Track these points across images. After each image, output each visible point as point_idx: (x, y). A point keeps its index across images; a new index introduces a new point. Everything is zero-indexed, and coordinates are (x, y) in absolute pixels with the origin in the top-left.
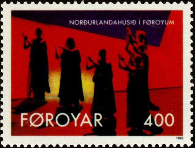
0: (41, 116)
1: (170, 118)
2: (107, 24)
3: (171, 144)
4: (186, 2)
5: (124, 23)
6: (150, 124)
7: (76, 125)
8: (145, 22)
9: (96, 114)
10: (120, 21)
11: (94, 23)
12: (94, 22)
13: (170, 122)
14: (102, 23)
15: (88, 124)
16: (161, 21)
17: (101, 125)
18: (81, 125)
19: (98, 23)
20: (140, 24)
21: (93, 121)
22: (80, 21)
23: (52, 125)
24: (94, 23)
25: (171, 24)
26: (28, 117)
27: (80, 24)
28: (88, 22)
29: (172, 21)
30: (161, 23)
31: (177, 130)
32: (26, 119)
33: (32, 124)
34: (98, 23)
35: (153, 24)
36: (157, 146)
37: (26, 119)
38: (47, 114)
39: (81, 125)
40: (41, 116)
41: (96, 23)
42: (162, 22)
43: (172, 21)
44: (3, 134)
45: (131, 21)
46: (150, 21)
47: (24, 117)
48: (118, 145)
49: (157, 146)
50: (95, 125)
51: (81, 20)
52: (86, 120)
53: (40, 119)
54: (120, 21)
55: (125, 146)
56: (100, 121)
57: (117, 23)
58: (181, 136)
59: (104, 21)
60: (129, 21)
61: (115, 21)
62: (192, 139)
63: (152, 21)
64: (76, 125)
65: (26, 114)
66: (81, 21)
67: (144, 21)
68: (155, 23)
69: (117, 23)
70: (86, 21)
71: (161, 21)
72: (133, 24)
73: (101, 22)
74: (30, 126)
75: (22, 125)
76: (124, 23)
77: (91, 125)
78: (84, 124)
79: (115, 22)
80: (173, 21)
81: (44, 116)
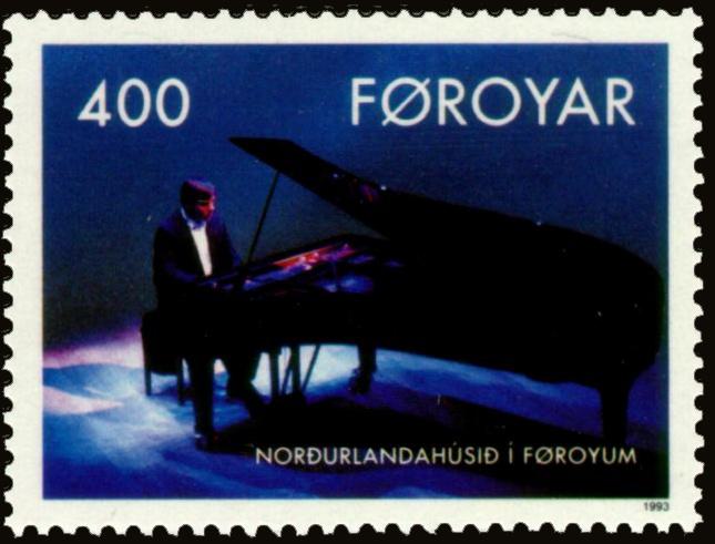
0: (421, 87)
1: (173, 95)
2: (393, 460)
5: (455, 458)
6: (102, 117)
7: (542, 120)
8: (530, 455)
9: (612, 83)
10: (439, 451)
11: (344, 457)
12: (344, 455)
13: (172, 110)
14: (374, 459)
15: (585, 117)
16: (590, 450)
17: (629, 120)
18: (561, 120)
19: (361, 458)
20: (511, 461)
21: (600, 109)
22: (293, 451)
23: (462, 121)
24: (344, 457)
25: (623, 459)
26: (375, 91)
27: (293, 459)
28: (323, 455)
29: (627, 452)
30: (589, 456)
32: (370, 99)
33: (391, 117)
34: (361, 458)
35: (299, 462)
37: (370, 99)
38: (443, 83)
39: (561, 120)
40: (421, 87)
41: (351, 458)
42: (594, 455)
43: (627, 452)
45: (480, 451)
46: (550, 451)
47: (364, 90)
50: (610, 120)
51: (298, 446)
52: (578, 102)
53: (419, 98)
54: (439, 451)
56: (628, 107)
57: (430, 457)
58: (662, 501)
59: (383, 452)
60: (470, 451)
61: (422, 451)
63: (558, 449)
64: (542, 120)
65: (370, 81)
66: (561, 452)
67: (526, 449)
68: (566, 457)
69: (430, 457)
70: (314, 449)
71: (590, 450)
72: (487, 462)
73: (370, 456)
74: (385, 123)
75: (355, 119)
76: (455, 458)
77: (595, 120)
78: (571, 117)
79: (370, 456)
80: (632, 452)
81: (433, 89)
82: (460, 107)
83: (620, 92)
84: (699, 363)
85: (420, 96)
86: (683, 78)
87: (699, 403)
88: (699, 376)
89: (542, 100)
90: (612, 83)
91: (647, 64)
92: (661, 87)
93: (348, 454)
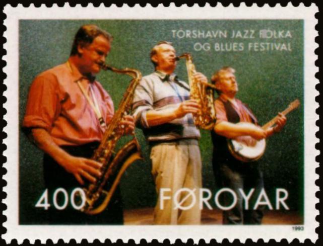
3: (189, 238)
4: (307, 4)
6: (46, 206)
7: (247, 207)
9: (278, 190)
15: (266, 206)
17: (286, 207)
18: (255, 208)
21: (273, 202)
23: (210, 207)
31: (294, 214)
32: (168, 198)
36: (49, 242)
37: (168, 198)
39: (255, 208)
44: (7, 222)
48: (149, 241)
49: (49, 242)
50: (278, 207)
55: (126, 241)
56: (286, 201)
58: (301, 226)
62: (317, 230)
77: (271, 207)
78: (260, 206)
82: (209, 201)
83: (282, 195)
84: (317, 93)
85: (191, 197)
86: (310, 34)
87: (317, 52)
88: (318, 218)
89: (247, 198)
90: (278, 190)
91: (298, 25)
92: (300, 159)
93: (190, 34)
